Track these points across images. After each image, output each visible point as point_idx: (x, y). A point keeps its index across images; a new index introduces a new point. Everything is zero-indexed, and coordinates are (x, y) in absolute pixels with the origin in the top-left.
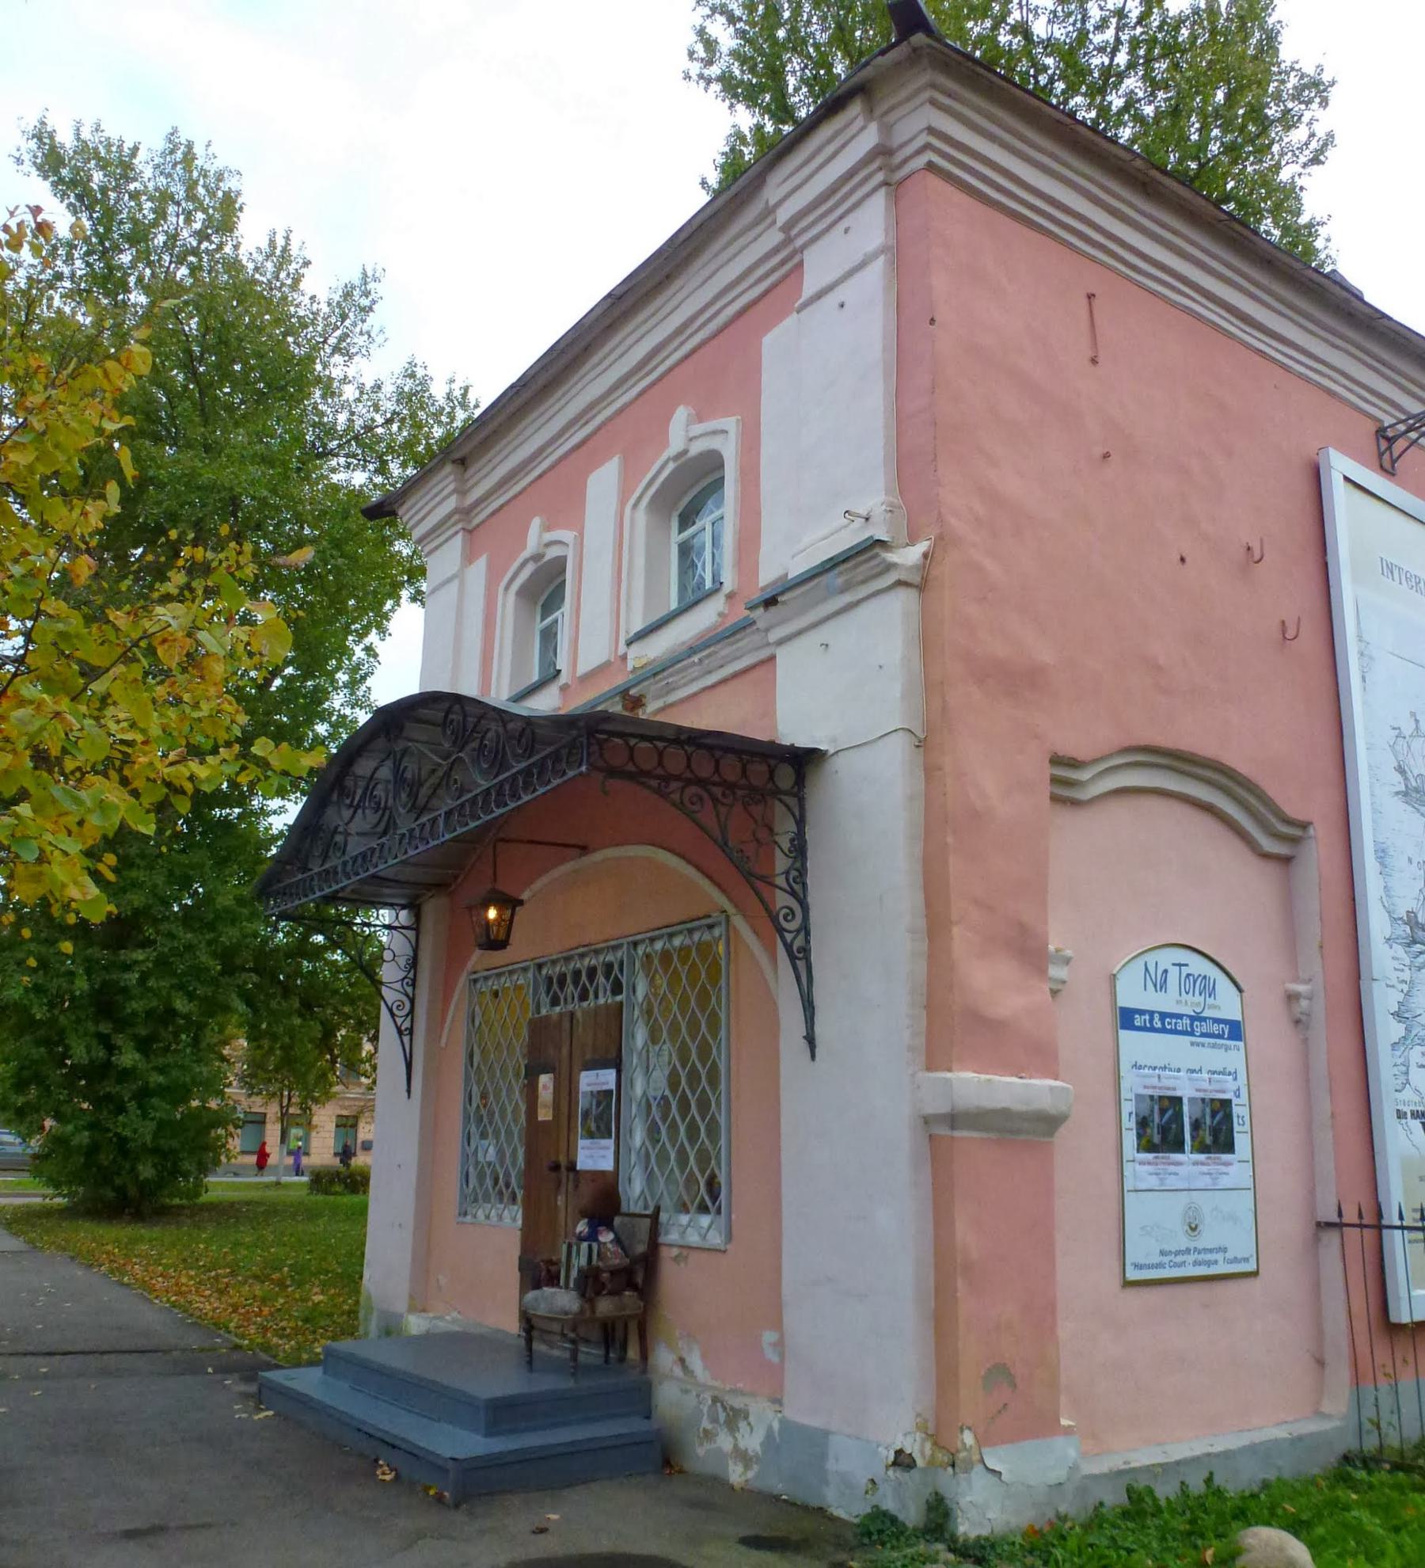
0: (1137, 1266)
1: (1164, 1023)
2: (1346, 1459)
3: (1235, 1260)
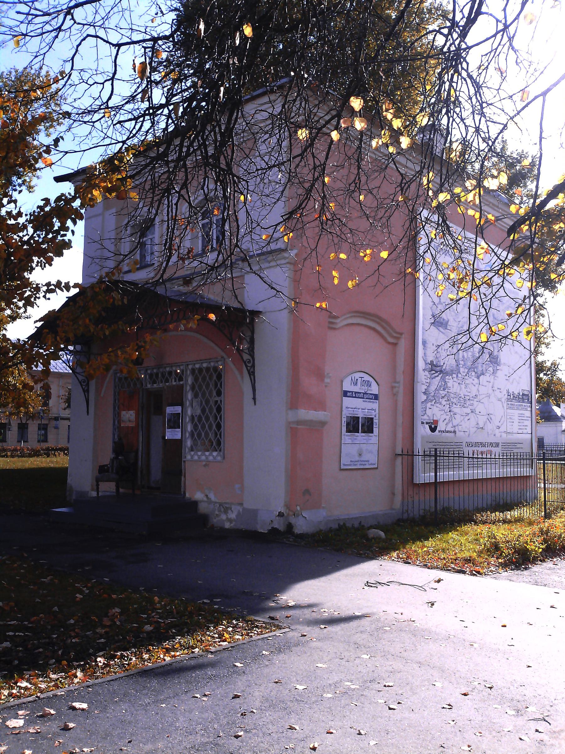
0: (344, 465)
1: (355, 395)
2: (399, 520)
3: (372, 464)
